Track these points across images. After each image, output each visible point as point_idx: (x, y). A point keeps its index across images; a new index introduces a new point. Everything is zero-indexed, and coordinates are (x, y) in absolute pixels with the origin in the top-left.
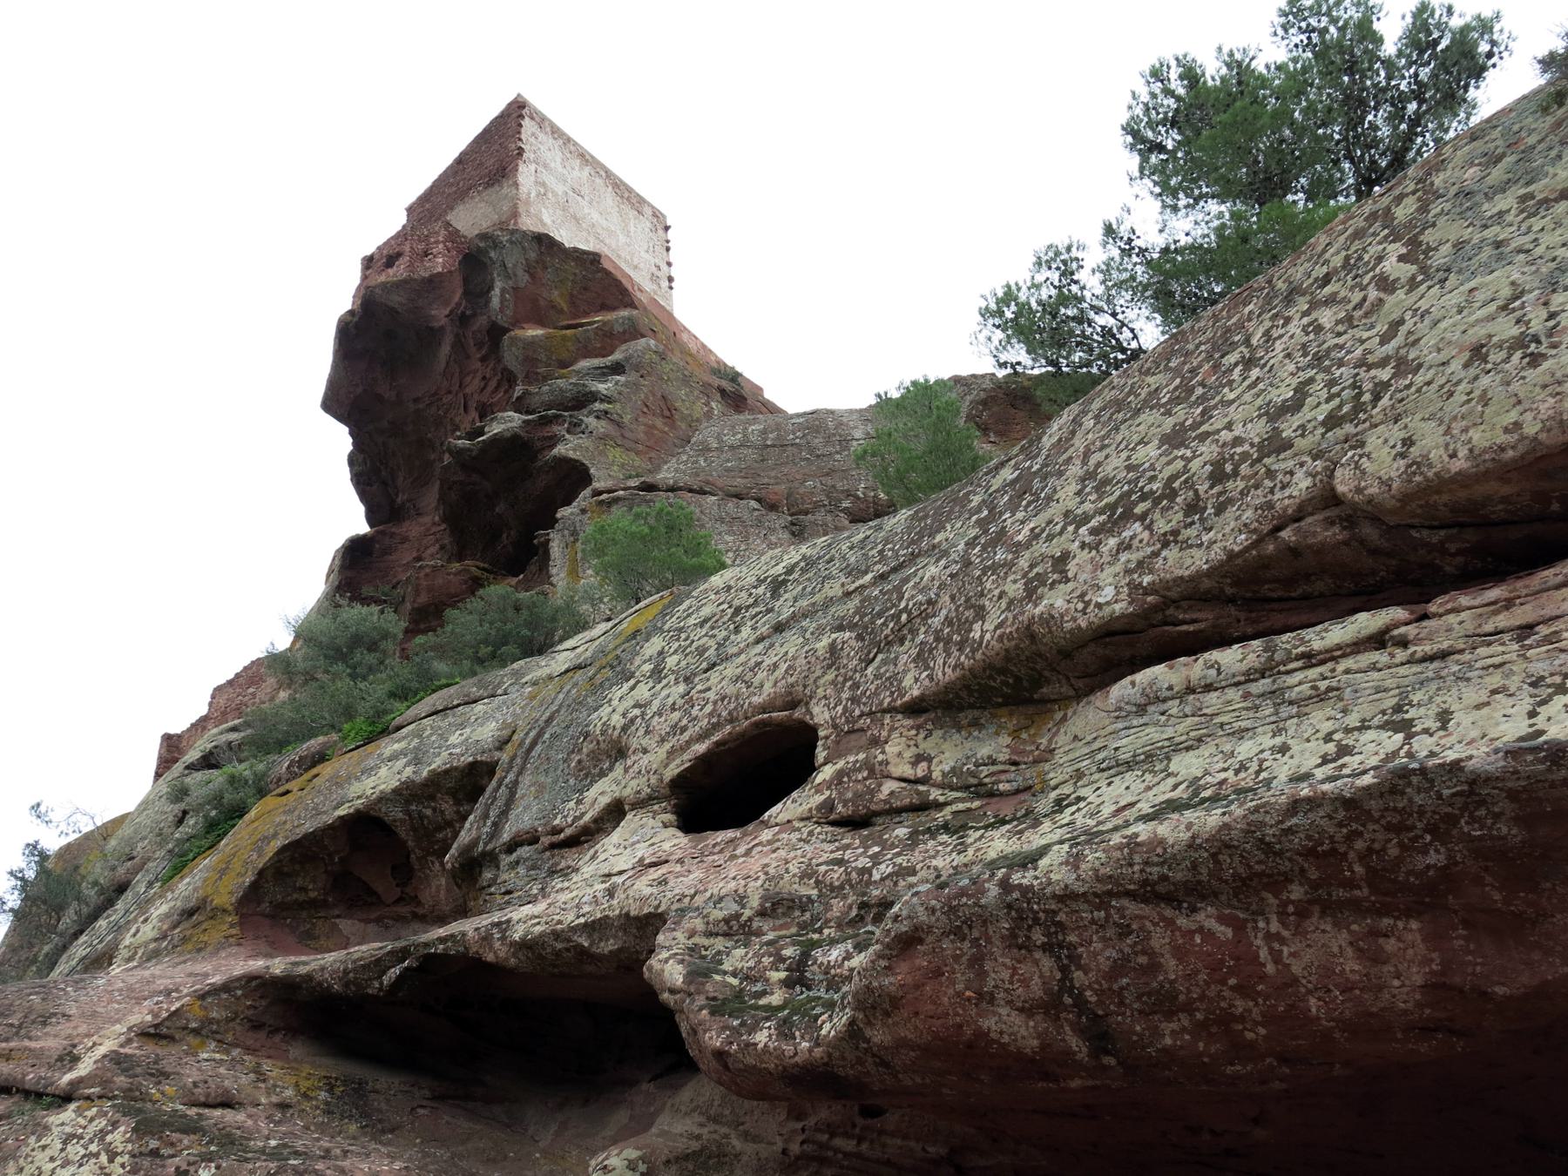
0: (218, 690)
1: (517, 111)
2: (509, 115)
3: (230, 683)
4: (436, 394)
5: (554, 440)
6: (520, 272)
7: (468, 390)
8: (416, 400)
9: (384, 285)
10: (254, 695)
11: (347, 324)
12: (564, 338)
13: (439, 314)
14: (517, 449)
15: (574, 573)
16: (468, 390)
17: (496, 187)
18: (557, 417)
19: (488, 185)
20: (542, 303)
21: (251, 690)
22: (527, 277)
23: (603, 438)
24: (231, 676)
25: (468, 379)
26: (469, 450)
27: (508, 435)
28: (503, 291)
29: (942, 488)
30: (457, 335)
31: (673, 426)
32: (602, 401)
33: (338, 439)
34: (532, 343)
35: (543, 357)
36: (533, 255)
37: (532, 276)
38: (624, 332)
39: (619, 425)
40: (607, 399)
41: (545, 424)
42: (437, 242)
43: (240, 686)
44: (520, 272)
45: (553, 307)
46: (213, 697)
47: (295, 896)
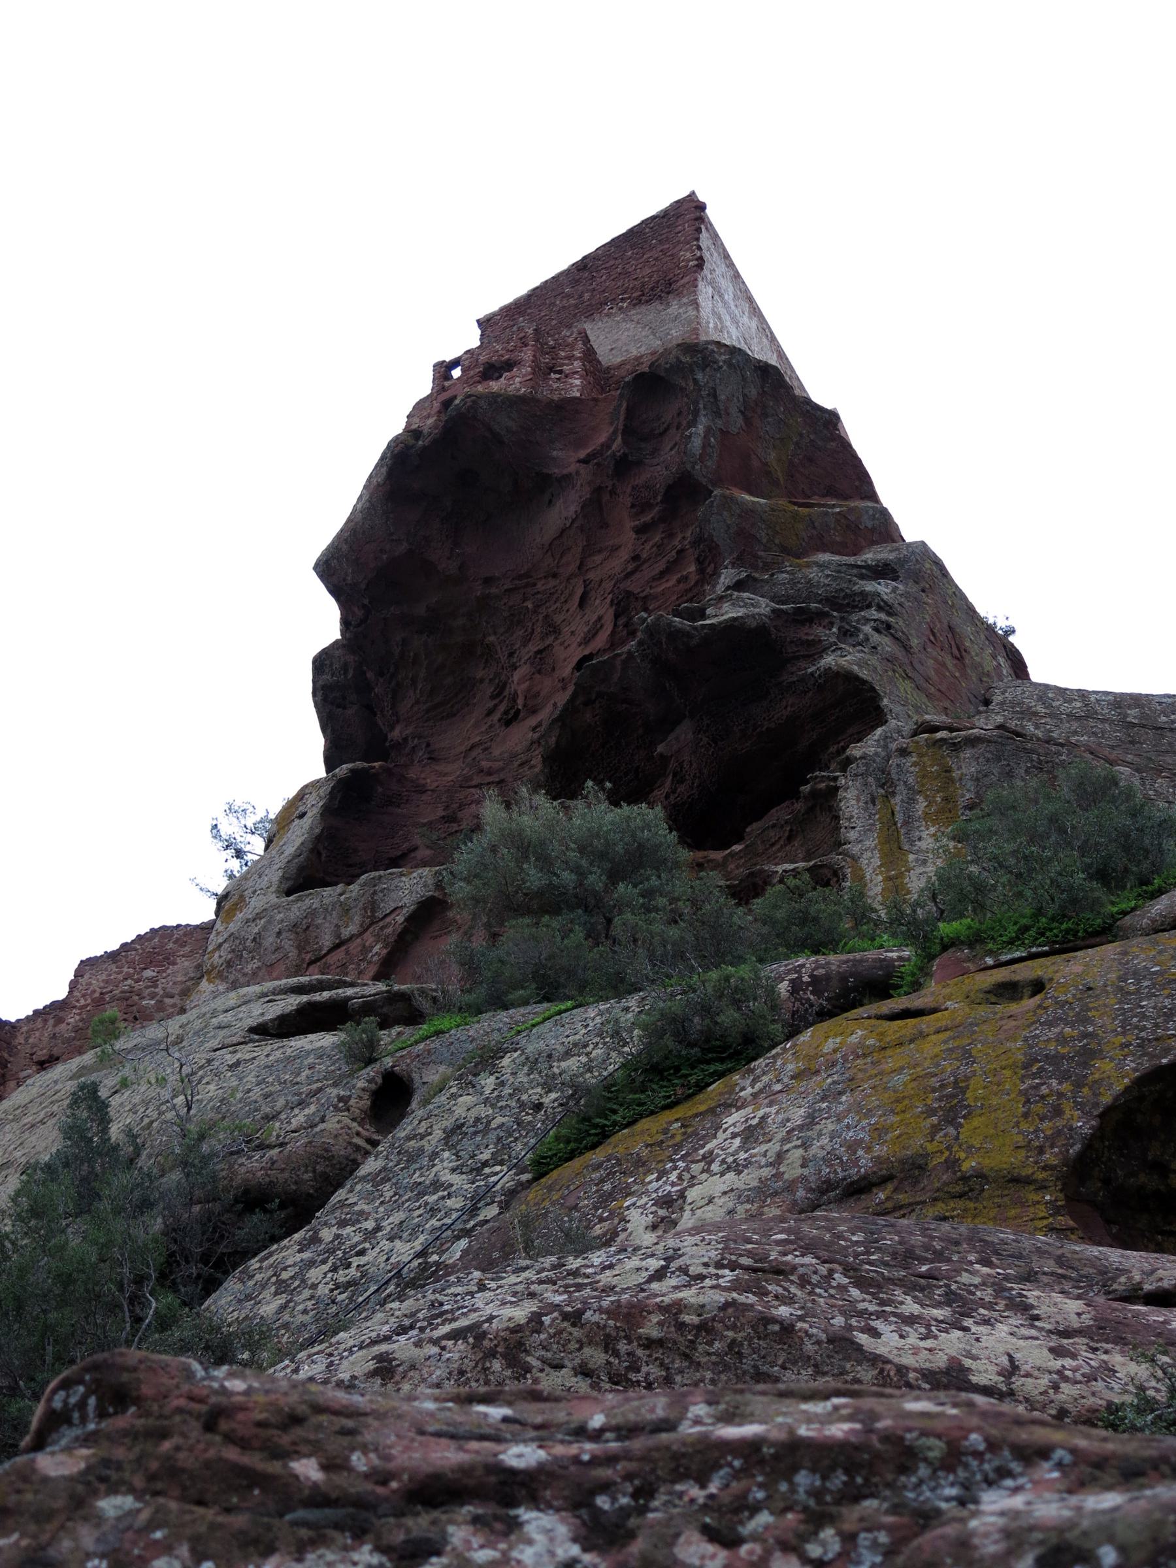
0: (87, 966)
1: (688, 216)
2: (678, 216)
3: (111, 956)
4: (527, 575)
5: (816, 649)
6: (734, 411)
7: (591, 575)
8: (488, 581)
9: (493, 398)
10: (154, 982)
11: (408, 447)
12: (795, 515)
13: (566, 458)
14: (754, 653)
15: (894, 845)
16: (591, 575)
17: (657, 305)
18: (821, 615)
19: (638, 302)
20: (755, 463)
21: (149, 973)
22: (740, 421)
23: (890, 660)
24: (115, 946)
25: (598, 558)
26: (688, 635)
27: (753, 624)
28: (708, 431)
29: (816, 952)
30: (598, 490)
31: (964, 674)
32: (880, 609)
33: (323, 621)
34: (749, 512)
35: (763, 535)
36: (753, 392)
37: (748, 421)
38: (873, 530)
39: (907, 648)
40: (884, 607)
41: (802, 623)
42: (571, 358)
43: (131, 964)
44: (734, 411)
45: (768, 473)
46: (79, 973)
47: (1143, 1178)
